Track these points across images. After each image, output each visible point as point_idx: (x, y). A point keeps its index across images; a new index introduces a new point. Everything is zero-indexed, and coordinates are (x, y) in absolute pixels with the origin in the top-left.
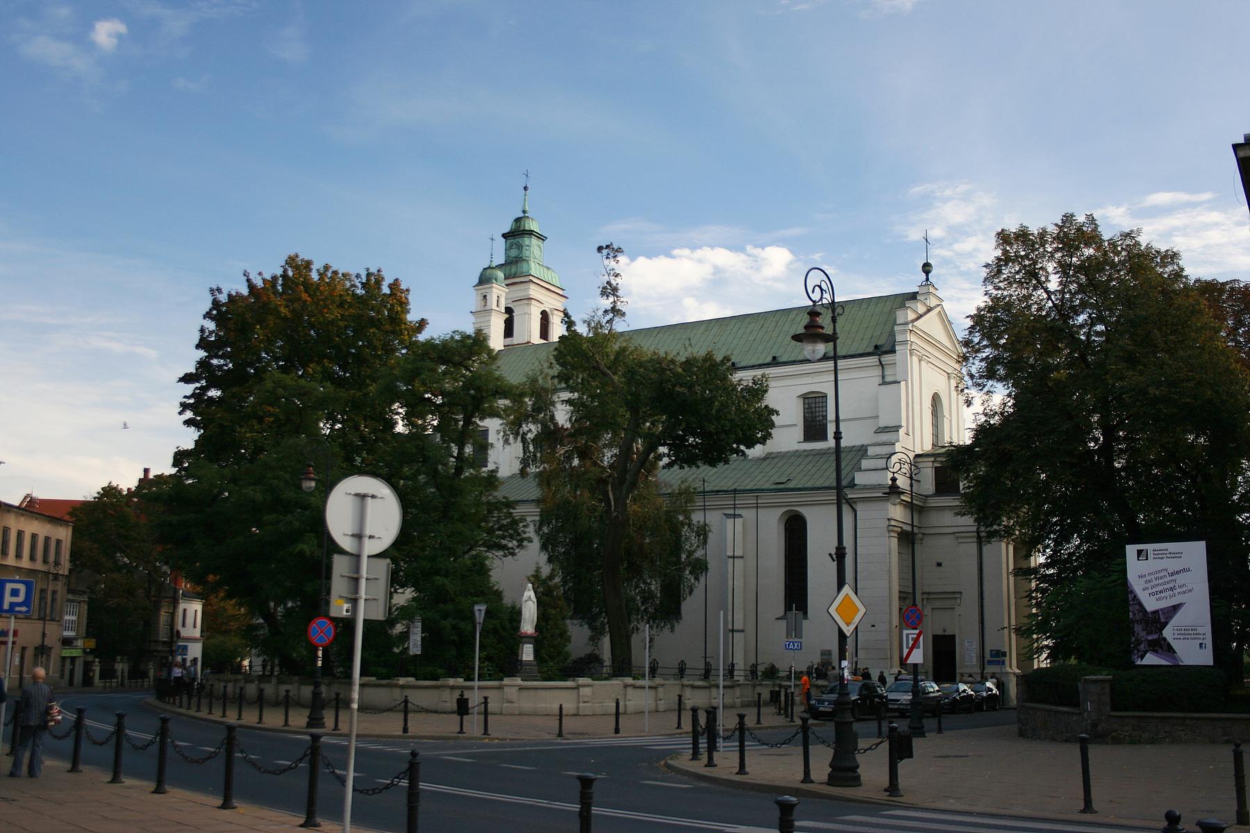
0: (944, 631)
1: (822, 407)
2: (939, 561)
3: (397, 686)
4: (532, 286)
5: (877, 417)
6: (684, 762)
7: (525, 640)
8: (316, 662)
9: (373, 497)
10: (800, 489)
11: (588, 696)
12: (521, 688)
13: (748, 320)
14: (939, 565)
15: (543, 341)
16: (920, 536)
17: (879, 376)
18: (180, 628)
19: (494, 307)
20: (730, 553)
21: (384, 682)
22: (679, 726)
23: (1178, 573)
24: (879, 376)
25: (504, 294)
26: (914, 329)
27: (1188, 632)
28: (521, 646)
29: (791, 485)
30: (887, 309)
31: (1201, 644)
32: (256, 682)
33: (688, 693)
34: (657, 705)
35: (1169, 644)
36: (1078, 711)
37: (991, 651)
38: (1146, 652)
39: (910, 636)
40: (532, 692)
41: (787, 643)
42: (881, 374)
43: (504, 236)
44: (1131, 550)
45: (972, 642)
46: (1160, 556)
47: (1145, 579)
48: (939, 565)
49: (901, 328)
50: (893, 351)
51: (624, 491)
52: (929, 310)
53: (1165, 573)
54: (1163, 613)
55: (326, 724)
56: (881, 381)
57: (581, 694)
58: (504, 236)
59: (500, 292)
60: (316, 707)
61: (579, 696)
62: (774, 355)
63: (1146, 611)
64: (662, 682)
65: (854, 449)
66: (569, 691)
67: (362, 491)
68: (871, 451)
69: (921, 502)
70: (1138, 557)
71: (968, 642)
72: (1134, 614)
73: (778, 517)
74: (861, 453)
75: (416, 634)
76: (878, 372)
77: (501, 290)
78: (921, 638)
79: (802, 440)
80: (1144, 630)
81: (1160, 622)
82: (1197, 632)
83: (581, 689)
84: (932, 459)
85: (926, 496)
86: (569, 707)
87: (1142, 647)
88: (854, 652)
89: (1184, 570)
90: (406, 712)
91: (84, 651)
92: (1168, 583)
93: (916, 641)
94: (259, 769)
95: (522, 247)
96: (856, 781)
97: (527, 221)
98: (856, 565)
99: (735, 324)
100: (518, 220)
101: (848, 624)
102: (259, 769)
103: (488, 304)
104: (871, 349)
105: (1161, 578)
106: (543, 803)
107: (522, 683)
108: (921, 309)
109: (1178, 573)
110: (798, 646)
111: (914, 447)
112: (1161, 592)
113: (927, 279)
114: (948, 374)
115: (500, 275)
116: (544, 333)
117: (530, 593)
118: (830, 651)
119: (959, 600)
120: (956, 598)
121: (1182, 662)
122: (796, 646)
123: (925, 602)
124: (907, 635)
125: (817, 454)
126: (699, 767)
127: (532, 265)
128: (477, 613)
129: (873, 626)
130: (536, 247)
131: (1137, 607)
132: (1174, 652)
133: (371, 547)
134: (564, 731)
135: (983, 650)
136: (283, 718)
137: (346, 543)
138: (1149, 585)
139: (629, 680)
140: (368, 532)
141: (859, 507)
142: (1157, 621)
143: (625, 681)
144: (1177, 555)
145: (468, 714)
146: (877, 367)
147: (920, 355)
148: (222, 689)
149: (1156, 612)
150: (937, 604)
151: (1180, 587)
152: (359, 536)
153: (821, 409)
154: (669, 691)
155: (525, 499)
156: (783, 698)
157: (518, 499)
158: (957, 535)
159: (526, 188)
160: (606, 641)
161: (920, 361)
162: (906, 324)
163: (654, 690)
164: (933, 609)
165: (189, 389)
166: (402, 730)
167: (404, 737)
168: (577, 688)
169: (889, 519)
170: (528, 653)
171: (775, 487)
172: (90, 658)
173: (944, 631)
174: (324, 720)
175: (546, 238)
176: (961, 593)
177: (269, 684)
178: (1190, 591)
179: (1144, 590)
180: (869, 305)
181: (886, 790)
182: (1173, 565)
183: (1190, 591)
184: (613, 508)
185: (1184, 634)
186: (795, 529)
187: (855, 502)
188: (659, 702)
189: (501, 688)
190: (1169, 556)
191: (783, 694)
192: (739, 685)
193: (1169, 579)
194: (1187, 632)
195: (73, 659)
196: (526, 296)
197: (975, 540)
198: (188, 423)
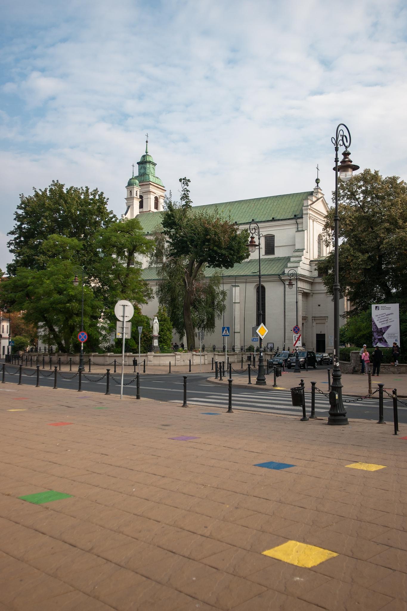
0: (321, 332)
2: (319, 304)
3: (107, 356)
4: (151, 186)
5: (295, 245)
6: (213, 379)
8: (81, 348)
9: (127, 306)
11: (179, 359)
12: (154, 356)
13: (242, 203)
14: (319, 305)
15: (155, 211)
16: (312, 294)
17: (296, 228)
18: (1, 333)
19: (135, 196)
20: (234, 301)
21: (102, 354)
22: (212, 369)
23: (389, 315)
24: (296, 228)
25: (139, 190)
26: (311, 208)
27: (391, 336)
30: (300, 199)
31: (396, 340)
32: (49, 356)
33: (217, 357)
34: (205, 362)
35: (385, 340)
36: (350, 363)
38: (377, 342)
39: (296, 337)
40: (158, 358)
43: (138, 163)
44: (373, 306)
45: (332, 337)
46: (383, 308)
47: (378, 317)
48: (319, 305)
49: (306, 208)
50: (302, 218)
51: (191, 279)
52: (318, 199)
53: (385, 315)
54: (384, 329)
55: (85, 370)
56: (297, 230)
58: (138, 163)
59: (137, 189)
60: (81, 363)
61: (176, 359)
62: (253, 219)
63: (378, 328)
64: (207, 353)
65: (285, 258)
66: (172, 357)
67: (124, 304)
69: (312, 280)
70: (376, 309)
71: (330, 337)
72: (374, 329)
73: (253, 288)
74: (288, 260)
75: (113, 336)
76: (295, 226)
77: (137, 188)
78: (301, 337)
79: (264, 254)
80: (377, 335)
81: (382, 332)
82: (395, 336)
85: (314, 278)
86: (173, 363)
87: (376, 341)
89: (391, 314)
90: (115, 365)
92: (386, 318)
93: (298, 338)
94: (90, 380)
95: (146, 168)
96: (265, 383)
97: (148, 157)
98: (285, 306)
99: (237, 205)
100: (144, 156)
101: (262, 336)
102: (90, 380)
103: (132, 195)
104: (293, 217)
105: (383, 316)
106: (170, 390)
107: (154, 354)
108: (314, 199)
109: (389, 315)
111: (310, 258)
112: (383, 321)
113: (318, 186)
115: (137, 182)
116: (156, 207)
117: (156, 320)
119: (327, 320)
120: (326, 319)
121: (389, 346)
123: (313, 320)
124: (295, 336)
126: (217, 381)
127: (151, 177)
128: (139, 330)
130: (152, 168)
131: (375, 327)
132: (387, 343)
133: (126, 319)
134: (171, 371)
136: (69, 369)
137: (121, 319)
138: (379, 319)
139: (194, 353)
140: (125, 315)
142: (381, 332)
144: (389, 308)
145: (137, 365)
146: (295, 224)
147: (313, 219)
149: (381, 328)
150: (318, 322)
151: (390, 320)
152: (123, 316)
153: (272, 242)
154: (208, 358)
155: (150, 279)
156: (252, 359)
157: (148, 279)
159: (147, 142)
160: (185, 338)
161: (313, 221)
162: (308, 206)
163: (203, 356)
164: (316, 323)
165: (13, 237)
166: (114, 371)
170: (156, 343)
171: (252, 274)
173: (321, 332)
174: (84, 369)
175: (156, 164)
176: (328, 317)
177: (54, 356)
178: (393, 321)
179: (377, 320)
180: (293, 197)
181: (273, 386)
182: (387, 312)
183: (393, 321)
184: (187, 286)
185: (391, 336)
186: (261, 292)
187: (285, 281)
188: (205, 361)
189: (147, 356)
190: (386, 308)
191: (252, 357)
192: (236, 354)
193: (386, 317)
194: (392, 336)
196: (148, 190)
198: (11, 251)
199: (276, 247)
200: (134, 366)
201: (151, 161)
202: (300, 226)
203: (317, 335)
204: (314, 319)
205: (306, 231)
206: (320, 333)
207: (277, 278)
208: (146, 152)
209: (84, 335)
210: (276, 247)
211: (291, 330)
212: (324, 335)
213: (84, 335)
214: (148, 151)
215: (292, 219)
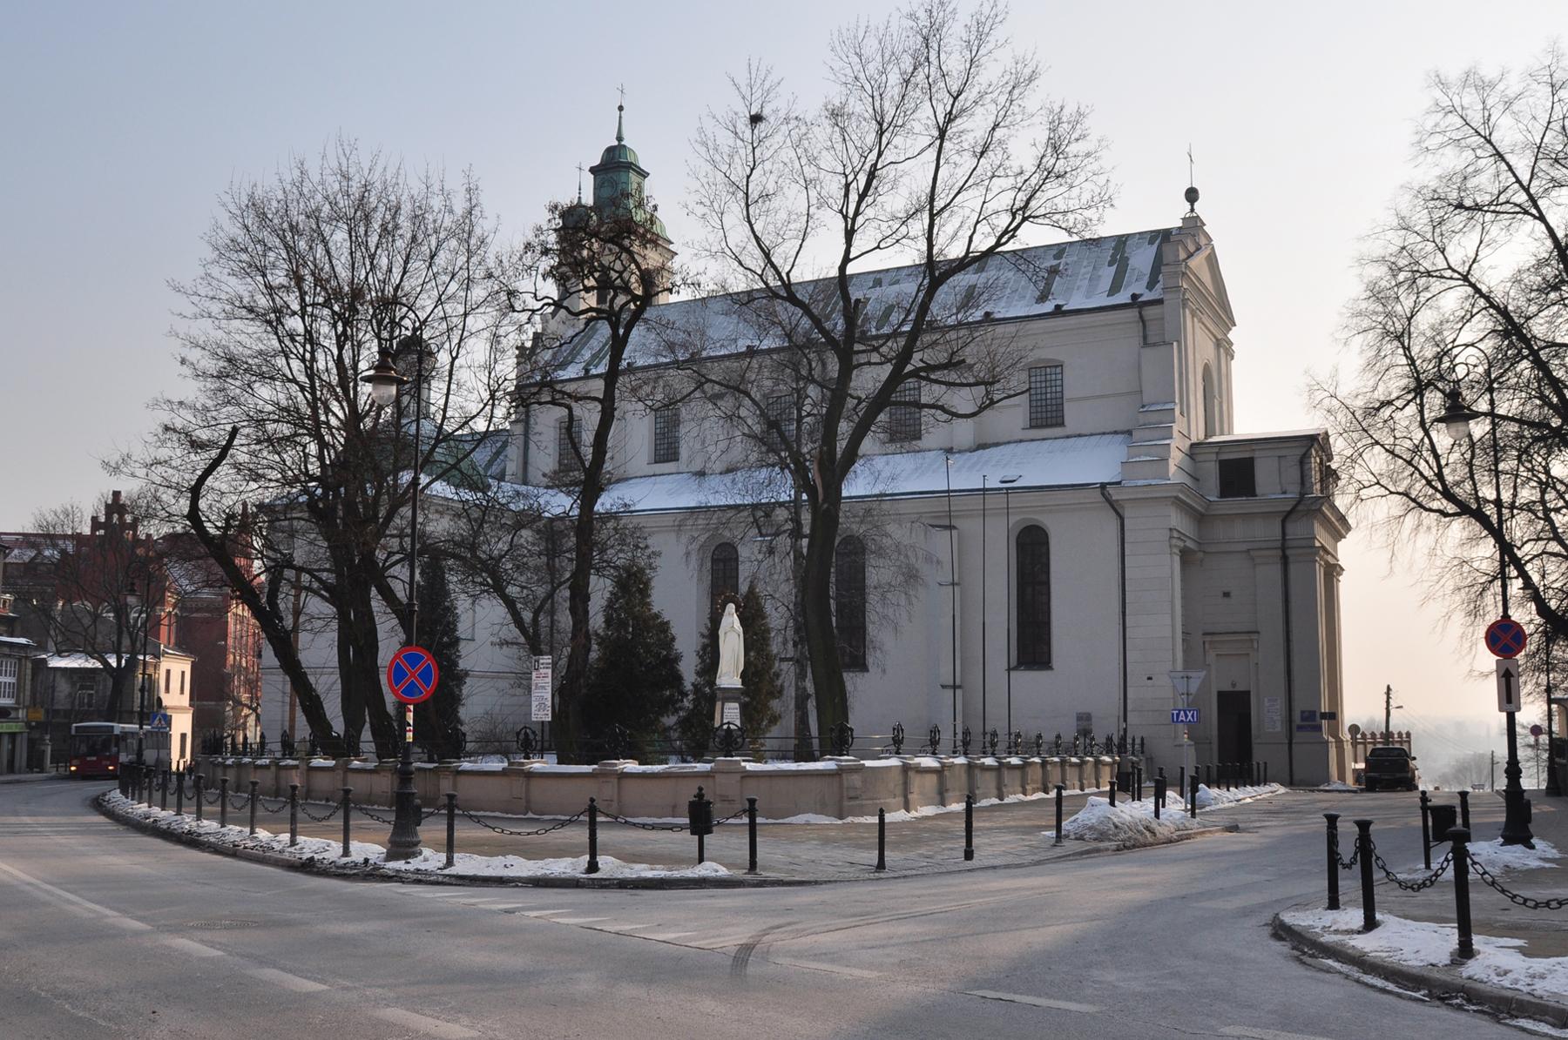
1: (1046, 381)
2: (1226, 590)
14: (1227, 595)
37: (1303, 712)
41: (1175, 712)
42: (1141, 334)
43: (592, 170)
48: (1227, 595)
57: (845, 784)
58: (592, 170)
71: (1269, 700)
83: (844, 776)
91: (28, 724)
110: (1193, 716)
113: (1192, 210)
114: (1217, 340)
118: (1089, 714)
122: (1190, 717)
123: (1207, 646)
158: (1252, 553)
159: (621, 108)
164: (1217, 655)
169: (1171, 529)
170: (731, 714)
172: (36, 735)
195: (13, 735)
199: (1070, 400)
201: (632, 163)
203: (1221, 694)
204: (1211, 642)
206: (1231, 689)
207: (1096, 495)
208: (619, 138)
209: (421, 667)
210: (1070, 400)
212: (1246, 695)
213: (421, 667)
214: (625, 134)
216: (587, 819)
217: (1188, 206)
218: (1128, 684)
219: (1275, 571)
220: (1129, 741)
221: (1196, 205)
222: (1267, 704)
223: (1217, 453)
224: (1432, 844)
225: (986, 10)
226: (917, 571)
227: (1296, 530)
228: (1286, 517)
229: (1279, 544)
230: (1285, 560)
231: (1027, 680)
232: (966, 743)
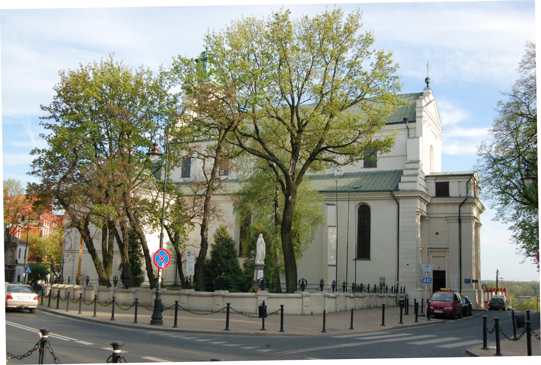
2: (437, 232)
5: (406, 155)
7: (259, 267)
10: (368, 191)
14: (437, 233)
18: (17, 258)
28: (256, 271)
29: (362, 189)
34: (336, 308)
37: (465, 279)
48: (437, 233)
50: (415, 121)
55: (164, 323)
68: (405, 172)
74: (400, 173)
76: (406, 132)
83: (304, 298)
84: (435, 178)
88: (397, 278)
96: (161, 323)
113: (428, 86)
119: (448, 252)
122: (428, 281)
123: (429, 252)
125: (372, 174)
129: (408, 265)
135: (461, 279)
141: (401, 202)
143: (304, 294)
148: (57, 293)
163: (335, 299)
167: (226, 333)
168: (302, 297)
187: (399, 199)
197: (457, 221)
200: (261, 319)
202: (411, 132)
204: (431, 251)
205: (420, 138)
211: (439, 268)
212: (444, 272)
215: (401, 123)
216: (431, 307)
217: (426, 84)
218: (399, 266)
219: (457, 224)
220: (399, 288)
221: (429, 84)
222: (452, 276)
223: (435, 180)
224: (516, 329)
225: (355, 13)
226: (171, 180)
227: (464, 209)
228: (461, 205)
229: (458, 215)
230: (460, 220)
231: (361, 263)
232: (333, 286)
